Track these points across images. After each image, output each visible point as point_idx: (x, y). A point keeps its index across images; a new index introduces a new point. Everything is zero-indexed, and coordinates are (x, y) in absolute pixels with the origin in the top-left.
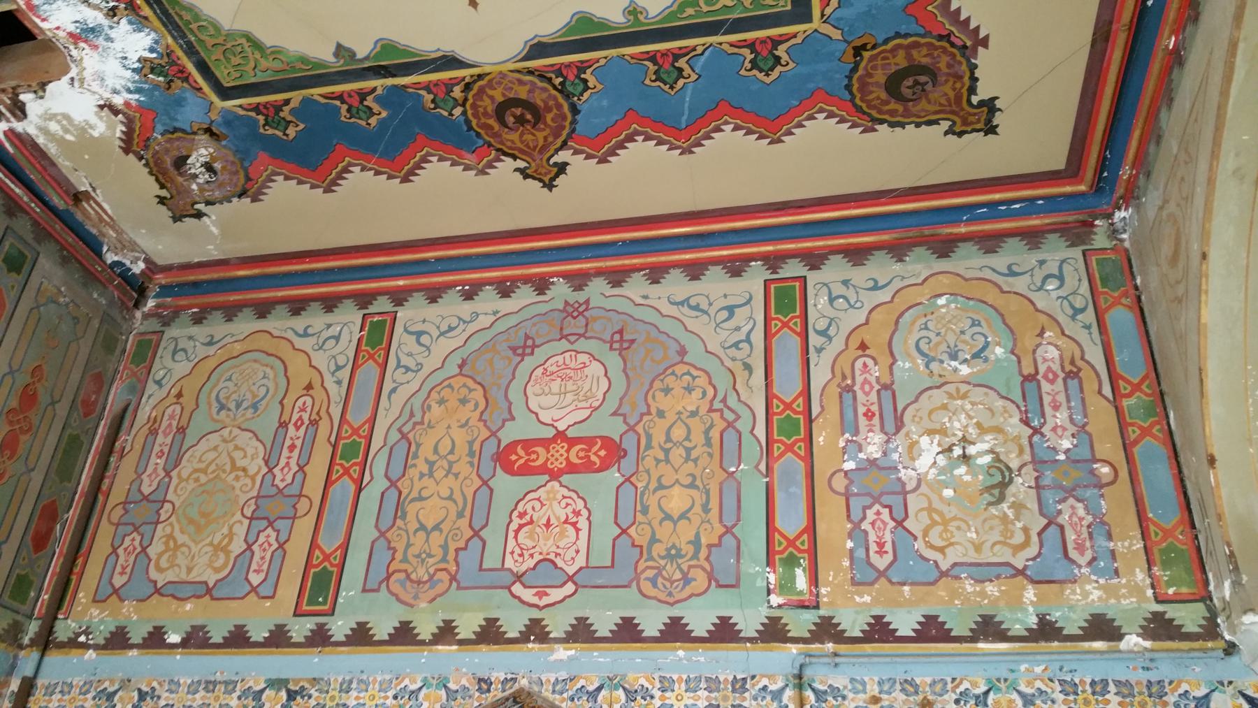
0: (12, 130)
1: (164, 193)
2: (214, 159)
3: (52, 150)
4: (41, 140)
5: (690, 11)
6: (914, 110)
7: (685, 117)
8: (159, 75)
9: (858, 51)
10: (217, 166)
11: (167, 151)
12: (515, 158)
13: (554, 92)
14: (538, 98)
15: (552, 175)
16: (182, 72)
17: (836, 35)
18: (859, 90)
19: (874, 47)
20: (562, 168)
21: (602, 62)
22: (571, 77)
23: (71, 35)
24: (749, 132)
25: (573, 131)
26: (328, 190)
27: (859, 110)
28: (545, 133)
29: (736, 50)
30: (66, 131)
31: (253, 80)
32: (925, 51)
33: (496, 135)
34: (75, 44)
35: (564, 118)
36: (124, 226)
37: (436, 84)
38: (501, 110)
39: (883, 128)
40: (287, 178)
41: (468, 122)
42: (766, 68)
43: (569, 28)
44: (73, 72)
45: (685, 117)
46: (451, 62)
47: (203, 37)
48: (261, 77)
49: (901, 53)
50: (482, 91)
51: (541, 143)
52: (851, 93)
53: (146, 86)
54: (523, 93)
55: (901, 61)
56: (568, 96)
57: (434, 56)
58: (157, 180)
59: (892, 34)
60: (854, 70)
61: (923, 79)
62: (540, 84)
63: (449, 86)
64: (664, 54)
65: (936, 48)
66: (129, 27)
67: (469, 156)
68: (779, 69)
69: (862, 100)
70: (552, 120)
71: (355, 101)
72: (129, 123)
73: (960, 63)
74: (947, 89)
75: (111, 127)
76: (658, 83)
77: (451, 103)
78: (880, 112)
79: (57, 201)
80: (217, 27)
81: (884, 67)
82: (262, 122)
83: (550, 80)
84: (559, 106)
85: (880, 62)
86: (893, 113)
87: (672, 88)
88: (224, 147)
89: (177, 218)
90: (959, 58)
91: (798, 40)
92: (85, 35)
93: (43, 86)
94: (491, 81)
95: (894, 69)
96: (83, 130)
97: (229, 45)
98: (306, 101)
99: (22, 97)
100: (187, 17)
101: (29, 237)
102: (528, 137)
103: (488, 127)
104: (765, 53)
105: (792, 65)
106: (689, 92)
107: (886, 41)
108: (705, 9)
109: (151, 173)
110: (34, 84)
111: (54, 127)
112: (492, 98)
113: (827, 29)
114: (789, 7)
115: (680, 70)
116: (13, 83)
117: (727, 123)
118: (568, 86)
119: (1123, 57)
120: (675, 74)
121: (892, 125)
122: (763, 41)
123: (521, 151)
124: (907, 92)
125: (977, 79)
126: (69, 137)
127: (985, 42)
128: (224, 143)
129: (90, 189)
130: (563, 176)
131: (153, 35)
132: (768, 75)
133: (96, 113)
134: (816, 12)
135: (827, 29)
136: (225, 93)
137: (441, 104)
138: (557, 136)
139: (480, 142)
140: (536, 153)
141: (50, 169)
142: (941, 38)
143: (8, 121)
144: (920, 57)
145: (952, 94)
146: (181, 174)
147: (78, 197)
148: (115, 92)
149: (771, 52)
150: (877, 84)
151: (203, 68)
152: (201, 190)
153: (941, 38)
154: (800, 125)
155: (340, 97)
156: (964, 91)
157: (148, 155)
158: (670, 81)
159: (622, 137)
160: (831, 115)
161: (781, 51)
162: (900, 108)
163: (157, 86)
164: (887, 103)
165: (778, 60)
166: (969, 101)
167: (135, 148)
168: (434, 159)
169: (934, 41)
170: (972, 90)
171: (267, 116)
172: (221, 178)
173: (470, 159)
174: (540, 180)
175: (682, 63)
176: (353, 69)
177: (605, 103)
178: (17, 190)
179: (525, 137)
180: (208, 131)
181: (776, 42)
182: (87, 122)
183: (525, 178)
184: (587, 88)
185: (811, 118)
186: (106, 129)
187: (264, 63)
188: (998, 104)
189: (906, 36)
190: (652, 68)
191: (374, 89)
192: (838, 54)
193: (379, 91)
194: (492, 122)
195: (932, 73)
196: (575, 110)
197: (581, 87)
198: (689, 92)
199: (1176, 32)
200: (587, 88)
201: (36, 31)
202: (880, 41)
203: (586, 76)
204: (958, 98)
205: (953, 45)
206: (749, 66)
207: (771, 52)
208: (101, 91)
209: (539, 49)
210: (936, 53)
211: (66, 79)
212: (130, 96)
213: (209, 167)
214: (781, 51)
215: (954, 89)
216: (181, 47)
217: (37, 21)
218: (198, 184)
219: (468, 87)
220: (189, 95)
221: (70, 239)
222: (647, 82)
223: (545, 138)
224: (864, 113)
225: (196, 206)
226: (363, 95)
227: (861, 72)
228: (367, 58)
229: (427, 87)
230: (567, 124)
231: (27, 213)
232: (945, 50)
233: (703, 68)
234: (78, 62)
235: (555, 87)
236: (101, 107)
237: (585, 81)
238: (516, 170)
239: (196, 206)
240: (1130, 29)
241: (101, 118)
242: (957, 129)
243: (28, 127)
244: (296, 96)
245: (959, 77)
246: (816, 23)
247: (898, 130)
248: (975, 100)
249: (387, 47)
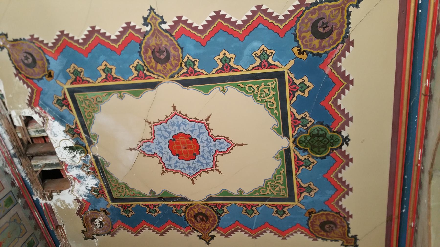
0: (46, 203)
1: (85, 230)
2: (104, 220)
3: (56, 211)
4: (53, 207)
5: (257, 193)
6: (329, 235)
7: (254, 226)
8: (95, 192)
9: (310, 213)
10: (104, 223)
11: (90, 216)
12: (198, 232)
13: (213, 212)
14: (208, 214)
15: (209, 239)
16: (103, 192)
17: (303, 207)
18: (311, 226)
19: (315, 213)
20: (213, 237)
21: (229, 205)
22: (219, 208)
23: (74, 178)
24: (275, 234)
25: (218, 225)
27: (311, 232)
28: (209, 225)
29: (271, 207)
30: (62, 205)
31: (123, 197)
32: (332, 216)
33: (193, 223)
34: (75, 180)
35: (216, 221)
36: (69, 239)
37: (178, 205)
38: (196, 215)
39: (320, 240)
40: (124, 230)
41: (185, 218)
42: (281, 214)
43: (220, 193)
44: (70, 189)
45: (254, 226)
46: (183, 199)
47: (112, 183)
48: (126, 197)
49: (324, 216)
50: (191, 208)
51: (207, 228)
52: (308, 226)
53: (91, 195)
54: (203, 211)
55: (324, 219)
56: (218, 214)
57: (179, 196)
58: (84, 225)
59: (321, 210)
60: (309, 219)
61: (332, 225)
62: (209, 209)
63: (181, 206)
64: (249, 205)
65: (335, 216)
66: (92, 178)
67: (183, 229)
68: (285, 215)
69: (312, 229)
70: (212, 221)
71: (152, 208)
72: (81, 206)
73: (344, 222)
74: (340, 230)
75: (76, 206)
76: (246, 214)
77: (181, 212)
78: (318, 234)
79: (51, 227)
80: (117, 180)
81: (319, 219)
82: (122, 210)
83: (213, 208)
84: (214, 217)
85: (317, 218)
86: (323, 235)
87: (251, 216)
88: (108, 217)
89: (86, 239)
90: (343, 220)
91: (291, 207)
92: (78, 178)
93: (60, 191)
94: (194, 206)
95: (322, 221)
96: (67, 206)
97: (119, 186)
98: (137, 206)
99: (53, 194)
100: (109, 176)
101: (38, 237)
102: (203, 225)
103: (191, 220)
104: (280, 209)
105: (289, 214)
106: (256, 218)
107: (319, 212)
108: (262, 193)
109: (83, 223)
110: (58, 190)
111: (59, 204)
112: (194, 211)
113: (300, 205)
114: (277, 79)
115: (254, 211)
116: (52, 189)
117: (268, 230)
118: (218, 211)
119: (398, 227)
120: (252, 212)
121: (323, 239)
122: (280, 206)
123: (200, 230)
124: (327, 229)
126: (62, 208)
127: (351, 216)
128: (108, 216)
129: (62, 225)
130: (213, 240)
131: (98, 180)
132: (281, 216)
133: (73, 202)
134: (296, 199)
135: (300, 205)
136: (113, 200)
137: (178, 211)
138: (212, 226)
139: (188, 225)
140: (205, 231)
141: (53, 217)
142: (337, 213)
143: (46, 200)
144: (331, 218)
145: (342, 232)
146: (92, 224)
147: (58, 227)
148: (81, 196)
149: (282, 209)
150: (317, 225)
151: (110, 192)
152: (97, 230)
153: (337, 213)
154: (292, 235)
155: (148, 206)
156: (346, 232)
157: (84, 217)
158: (250, 213)
159: (233, 229)
160: (302, 233)
161: (285, 209)
162: (325, 234)
163: (94, 195)
164: (320, 231)
165: (284, 212)
166: (348, 235)
167: (81, 214)
168: (172, 229)
169: (335, 214)
170: (349, 232)
171: (124, 209)
172: (104, 227)
173: (184, 230)
174: (205, 241)
175: (254, 208)
176: (154, 197)
177: (229, 218)
178: (41, 222)
179: (202, 225)
180: (105, 211)
181: (284, 207)
182: (69, 204)
183: (200, 239)
184: (224, 212)
185: (296, 232)
186: (74, 207)
187: (128, 193)
188: (358, 237)
189: (325, 211)
190: (245, 209)
191: (159, 204)
192: (304, 213)
193: (160, 205)
194: (193, 219)
195: (335, 224)
196: (219, 219)
197: (222, 212)
198: (256, 218)
199: (413, 221)
200: (224, 212)
201: (64, 176)
202: (317, 211)
203: (224, 208)
204: (344, 234)
205: (341, 216)
206: (275, 213)
207: (282, 209)
208: (76, 195)
209: (210, 198)
210: (336, 218)
211: (68, 190)
212: (85, 198)
213: (101, 223)
214: (285, 209)
215: (343, 231)
216: (105, 185)
217: (66, 173)
218: (96, 228)
219: (187, 207)
220: (103, 200)
221: (50, 240)
222: (243, 213)
223: (209, 226)
224: (313, 234)
225: (93, 235)
226: (155, 206)
227: (311, 220)
228: (158, 195)
229: (175, 206)
230: (216, 223)
231: (41, 229)
232: (338, 217)
233: (261, 211)
234: (73, 186)
235: (214, 211)
236: (75, 200)
237: (224, 210)
238: (198, 236)
239: (93, 235)
240: (398, 218)
241: (74, 203)
242: (345, 244)
243: (51, 203)
244: (134, 204)
245: (344, 227)
246: (296, 203)
247: (325, 241)
248: (350, 235)
249: (165, 192)
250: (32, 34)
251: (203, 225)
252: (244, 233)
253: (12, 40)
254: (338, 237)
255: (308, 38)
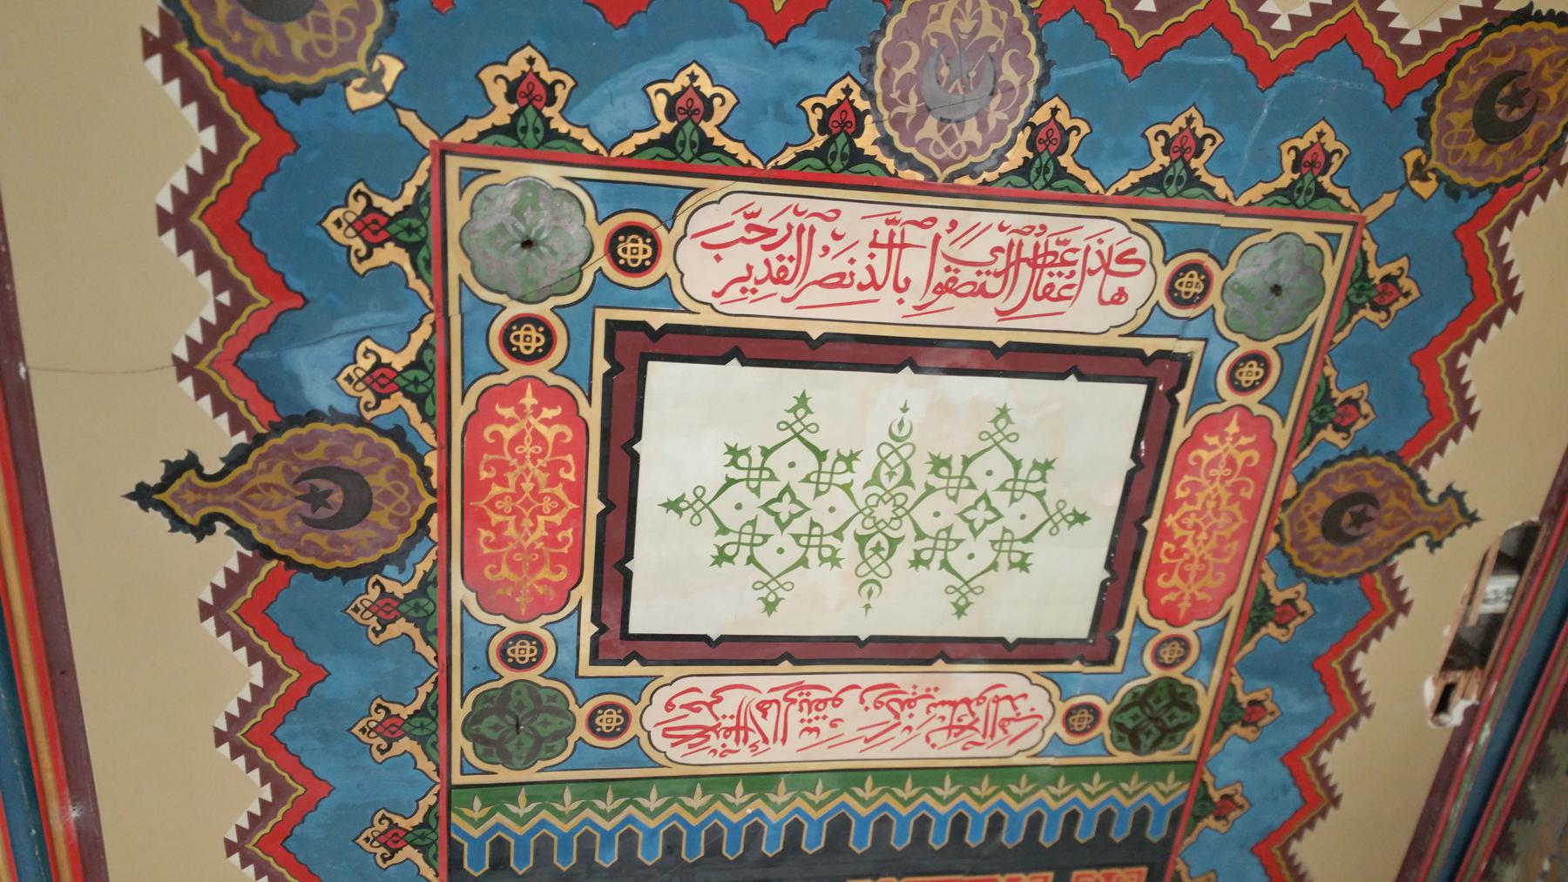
26: (1335, 802)
38: (1332, 530)
125: (1551, 12)
137: (1388, 300)
140: (1414, 518)
166: (1428, 503)
188: (1458, 487)
195: (1368, 498)
250: (153, 222)
251: (1387, 518)
252: (1538, 199)
253: (222, 465)
254: (1401, 535)
255: (311, 35)
